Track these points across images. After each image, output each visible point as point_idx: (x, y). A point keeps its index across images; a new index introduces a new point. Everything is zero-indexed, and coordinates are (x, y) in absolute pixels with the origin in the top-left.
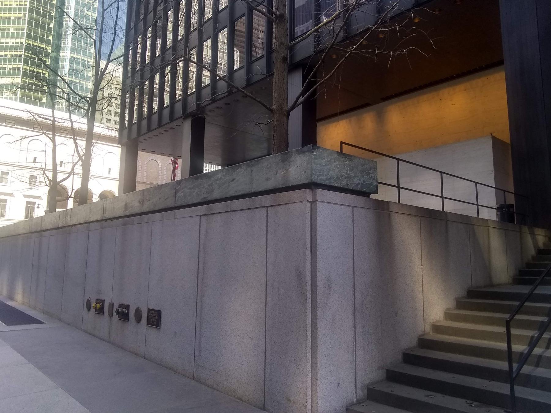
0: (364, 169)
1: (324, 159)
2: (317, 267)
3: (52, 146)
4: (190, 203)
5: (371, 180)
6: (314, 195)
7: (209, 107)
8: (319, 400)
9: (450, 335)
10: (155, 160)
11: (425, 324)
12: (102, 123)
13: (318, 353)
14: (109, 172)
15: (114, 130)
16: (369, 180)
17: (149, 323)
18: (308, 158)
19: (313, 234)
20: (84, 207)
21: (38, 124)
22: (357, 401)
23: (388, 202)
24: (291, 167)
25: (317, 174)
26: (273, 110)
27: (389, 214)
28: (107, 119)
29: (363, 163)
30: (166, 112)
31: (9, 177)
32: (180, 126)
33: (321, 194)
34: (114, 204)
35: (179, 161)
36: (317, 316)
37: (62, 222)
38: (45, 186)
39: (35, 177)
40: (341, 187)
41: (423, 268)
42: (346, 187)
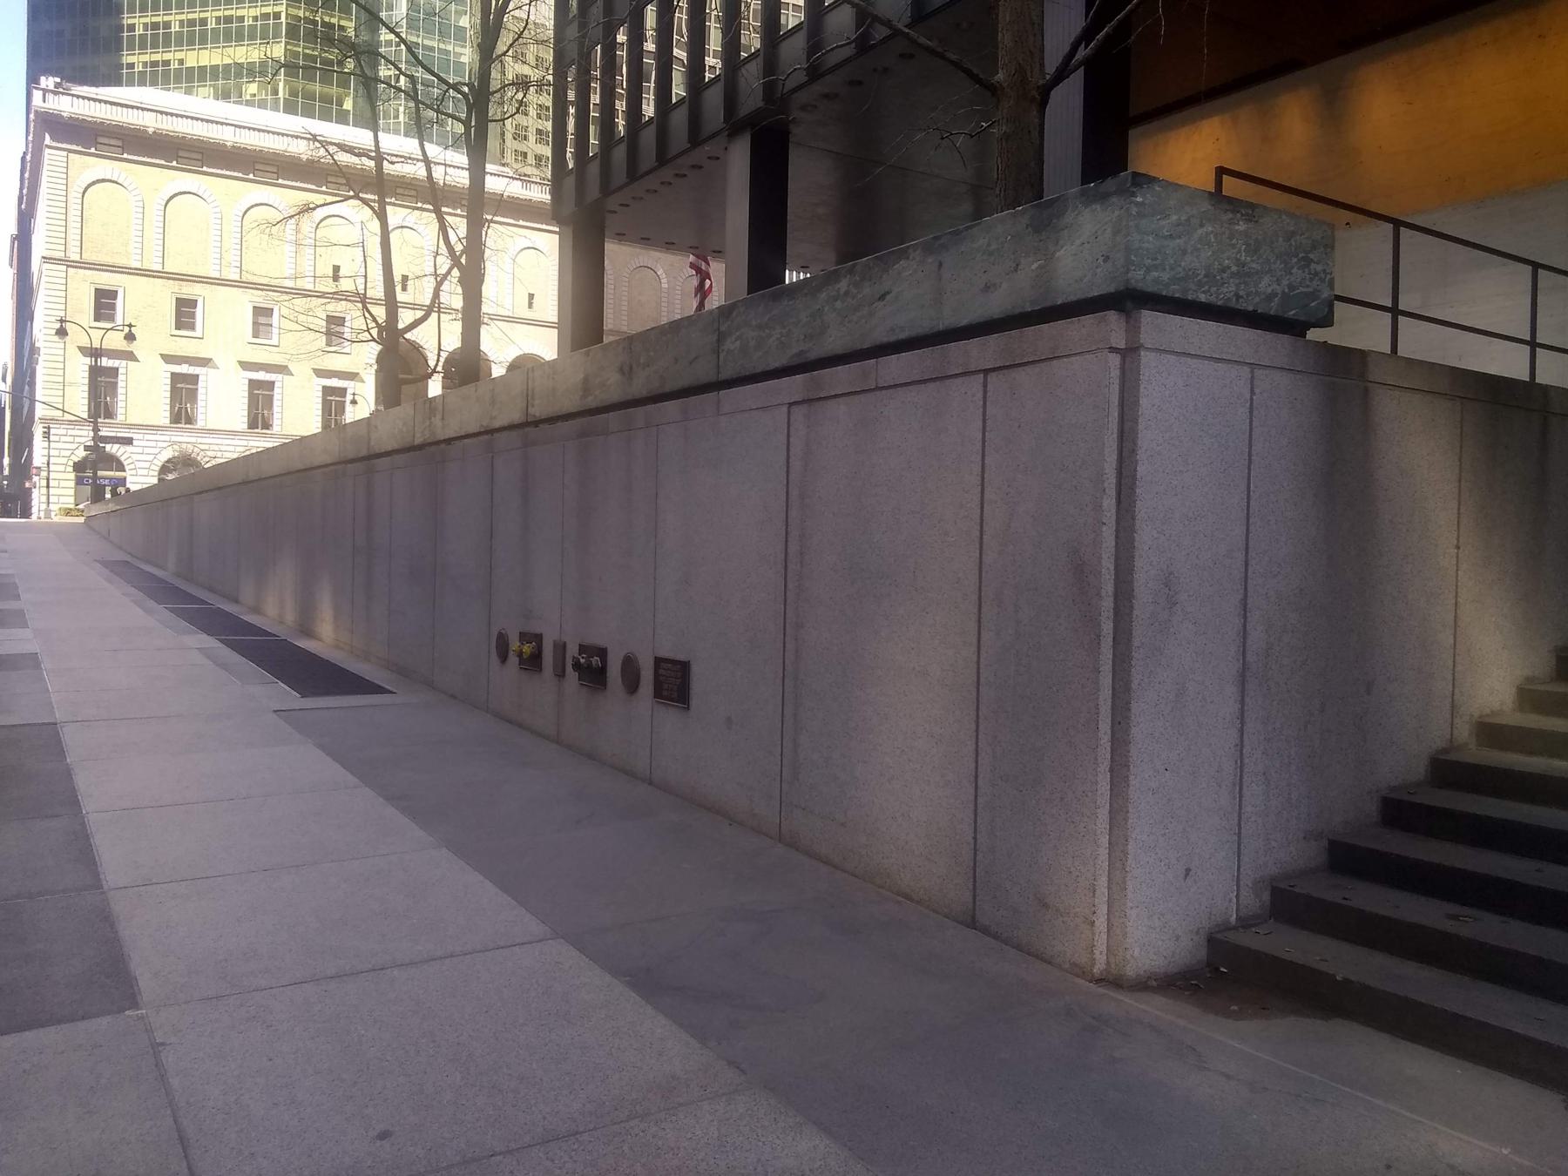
0: (1293, 249)
1: (1167, 216)
2: (1136, 544)
3: (378, 231)
4: (759, 370)
5: (1314, 282)
6: (1133, 329)
7: (802, 97)
8: (1132, 908)
9: (1531, 753)
10: (648, 268)
11: (1456, 721)
12: (503, 165)
13: (1132, 782)
14: (530, 305)
15: (536, 183)
16: (1308, 283)
17: (658, 693)
18: (1117, 213)
19: (1124, 449)
20: (476, 391)
21: (343, 173)
22: (1239, 918)
23: (1364, 351)
24: (1062, 247)
25: (1144, 265)
26: (998, 85)
27: (1366, 391)
28: (516, 151)
29: (1292, 228)
30: (679, 119)
31: (275, 319)
32: (718, 158)
33: (1155, 325)
34: (553, 378)
35: (717, 269)
36: (1131, 681)
37: (422, 432)
38: (369, 343)
39: (340, 321)
40: (1220, 303)
41: (1460, 555)
42: (1233, 304)
